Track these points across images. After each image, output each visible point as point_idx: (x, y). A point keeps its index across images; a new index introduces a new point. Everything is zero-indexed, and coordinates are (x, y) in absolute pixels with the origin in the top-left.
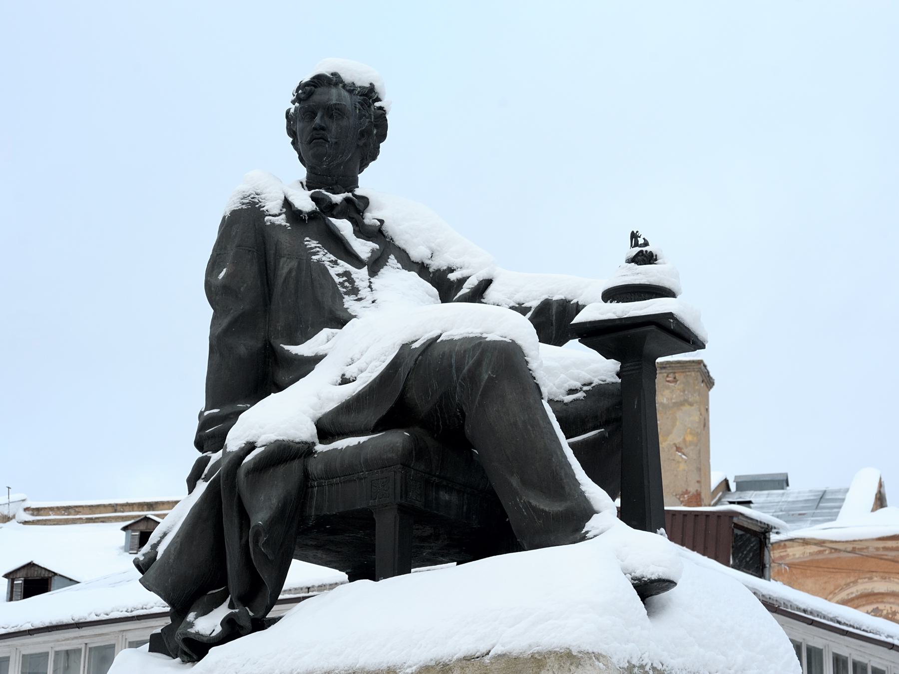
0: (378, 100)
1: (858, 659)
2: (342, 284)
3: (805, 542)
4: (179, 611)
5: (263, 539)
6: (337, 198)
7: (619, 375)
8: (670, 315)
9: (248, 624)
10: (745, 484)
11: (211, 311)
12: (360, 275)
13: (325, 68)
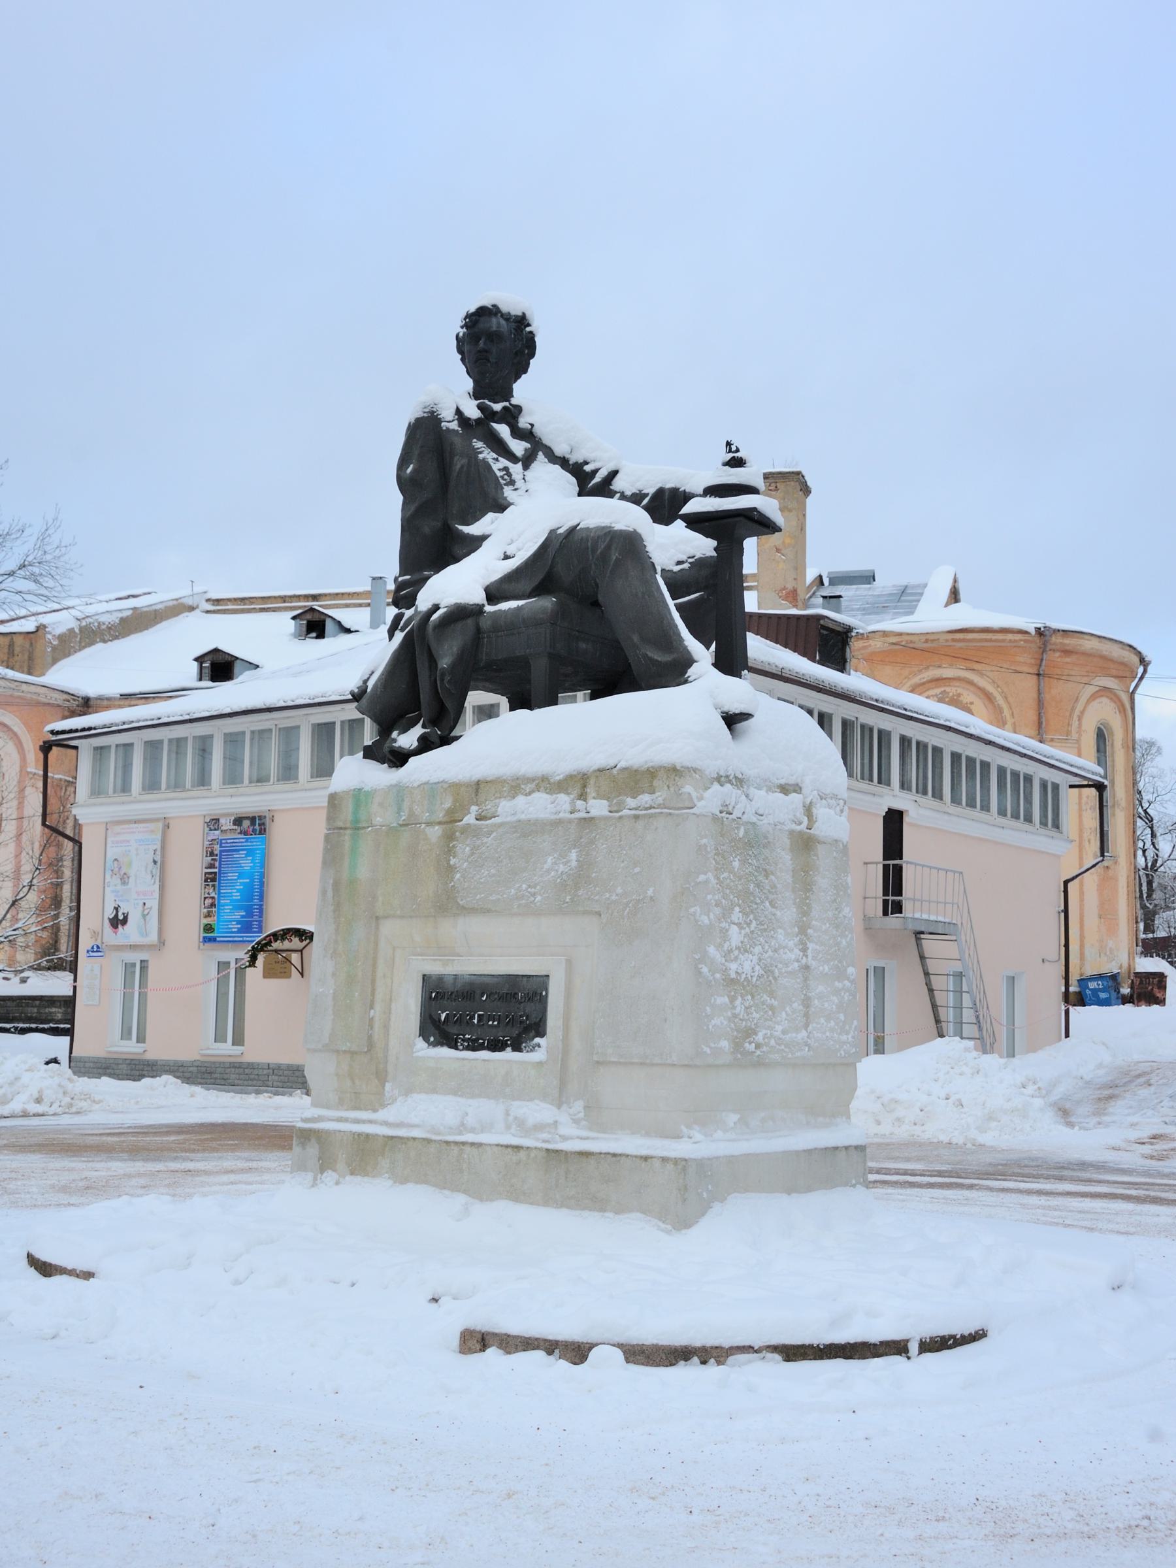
0: (529, 325)
1: (921, 739)
2: (502, 477)
3: (885, 634)
4: (385, 731)
5: (447, 678)
6: (497, 407)
7: (715, 549)
8: (755, 509)
9: (437, 741)
10: (836, 580)
11: (400, 498)
12: (516, 469)
13: (487, 302)
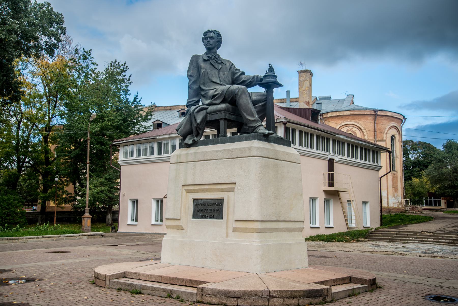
10: (320, 99)
